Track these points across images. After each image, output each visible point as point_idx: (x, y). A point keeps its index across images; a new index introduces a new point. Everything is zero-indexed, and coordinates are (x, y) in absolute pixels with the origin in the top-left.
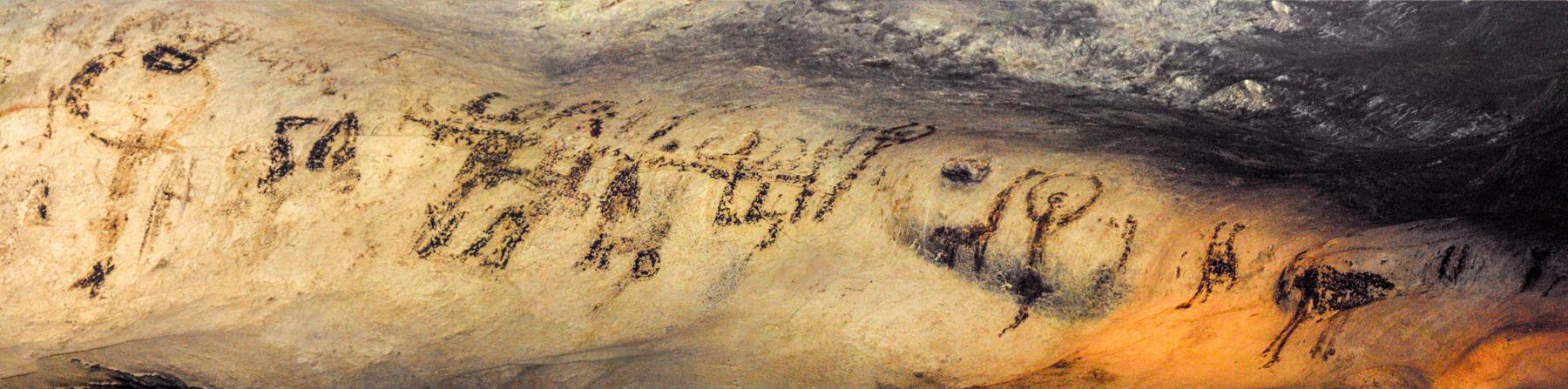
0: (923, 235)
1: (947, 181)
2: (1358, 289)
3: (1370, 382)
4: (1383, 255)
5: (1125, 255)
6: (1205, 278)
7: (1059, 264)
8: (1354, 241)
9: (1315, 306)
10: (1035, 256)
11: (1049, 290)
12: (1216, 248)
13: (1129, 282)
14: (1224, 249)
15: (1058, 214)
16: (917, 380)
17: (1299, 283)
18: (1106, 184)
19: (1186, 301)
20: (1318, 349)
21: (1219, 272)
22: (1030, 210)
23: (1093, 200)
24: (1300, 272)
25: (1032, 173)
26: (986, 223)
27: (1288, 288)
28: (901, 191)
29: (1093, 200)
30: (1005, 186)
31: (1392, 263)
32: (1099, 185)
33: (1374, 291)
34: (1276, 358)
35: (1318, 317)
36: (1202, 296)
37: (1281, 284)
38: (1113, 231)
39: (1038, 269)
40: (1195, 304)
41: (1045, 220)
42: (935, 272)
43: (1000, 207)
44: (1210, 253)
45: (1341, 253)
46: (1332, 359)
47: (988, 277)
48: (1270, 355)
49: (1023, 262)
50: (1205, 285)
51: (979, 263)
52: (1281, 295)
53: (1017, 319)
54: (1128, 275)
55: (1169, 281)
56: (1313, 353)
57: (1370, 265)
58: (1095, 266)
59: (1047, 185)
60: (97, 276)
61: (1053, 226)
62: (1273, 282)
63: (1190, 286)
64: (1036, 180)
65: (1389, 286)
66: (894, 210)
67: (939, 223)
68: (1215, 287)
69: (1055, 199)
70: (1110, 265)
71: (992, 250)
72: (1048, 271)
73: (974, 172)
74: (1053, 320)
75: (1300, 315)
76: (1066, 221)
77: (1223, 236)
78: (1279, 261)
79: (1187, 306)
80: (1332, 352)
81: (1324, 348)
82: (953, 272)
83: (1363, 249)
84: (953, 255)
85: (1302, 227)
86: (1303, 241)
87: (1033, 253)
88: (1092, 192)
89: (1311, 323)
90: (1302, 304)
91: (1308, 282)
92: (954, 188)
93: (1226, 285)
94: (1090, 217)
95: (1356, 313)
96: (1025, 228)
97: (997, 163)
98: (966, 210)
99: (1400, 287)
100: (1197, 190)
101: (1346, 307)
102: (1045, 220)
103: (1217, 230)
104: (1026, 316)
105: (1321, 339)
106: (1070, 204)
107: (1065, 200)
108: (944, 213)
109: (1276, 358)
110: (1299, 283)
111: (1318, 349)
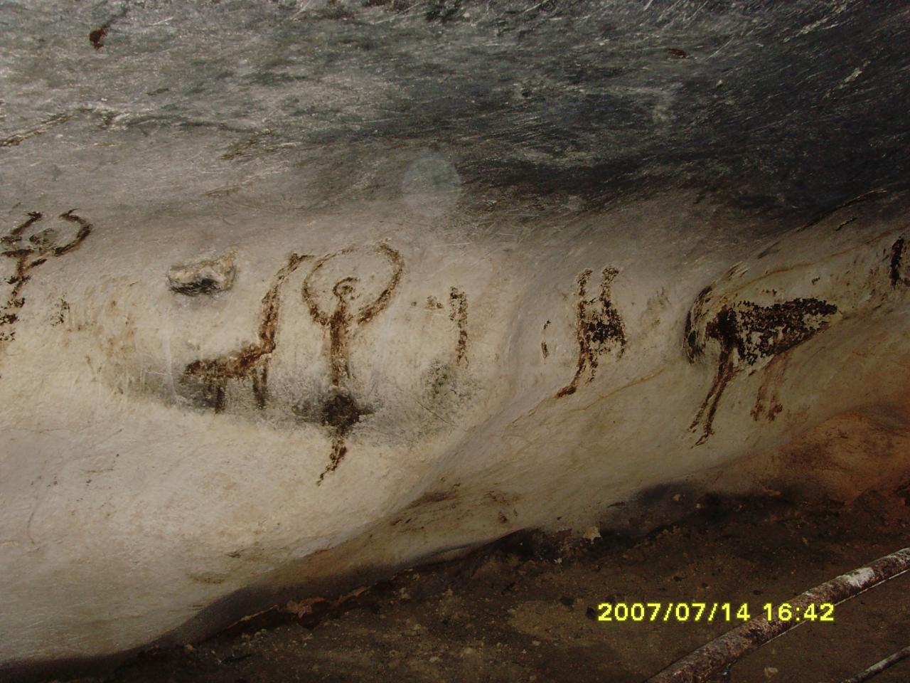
0: (169, 377)
1: (181, 298)
2: (789, 324)
3: (835, 434)
4: (812, 273)
5: (461, 342)
6: (584, 349)
7: (376, 374)
8: (771, 263)
9: (743, 356)
10: (338, 372)
11: (368, 411)
12: (588, 308)
13: (476, 376)
14: (599, 307)
15: (354, 309)
16: (235, 561)
17: (713, 331)
18: (404, 252)
19: (567, 384)
20: (760, 408)
21: (601, 338)
22: (314, 311)
23: (396, 279)
24: (711, 317)
25: (294, 261)
26: (258, 341)
27: (701, 340)
28: (112, 326)
29: (396, 279)
30: (266, 287)
31: (826, 280)
32: (395, 256)
33: (812, 321)
34: (708, 430)
35: (750, 369)
36: (587, 373)
37: (691, 338)
38: (437, 314)
39: (347, 387)
40: (581, 385)
41: (338, 319)
42: (201, 422)
43: (270, 317)
44: (582, 316)
45: (760, 285)
46: (780, 417)
47: (278, 412)
48: (700, 429)
49: (325, 382)
50: (586, 357)
51: (261, 397)
52: (693, 350)
53: (333, 458)
54: (473, 368)
55: (535, 364)
56: (755, 415)
57: (799, 290)
58: (425, 366)
59: (325, 271)
60: (40, 478)
61: (353, 327)
62: (677, 335)
63: (566, 364)
64: (304, 269)
65: (828, 310)
66: (110, 354)
67: (190, 358)
68: (601, 359)
69: (344, 288)
70: (446, 360)
71: (277, 376)
72: (362, 387)
73: (220, 278)
74: (384, 449)
75: (725, 372)
76: (368, 315)
77: (593, 291)
78: (677, 307)
79: (572, 390)
80: (778, 409)
81: (768, 405)
82: (223, 417)
83: (785, 270)
84: (220, 394)
85: (692, 254)
86: (702, 271)
87: (335, 368)
88: (390, 269)
89: (742, 377)
90: (724, 357)
91: (725, 328)
92: (195, 307)
93: (614, 352)
94: (397, 304)
95: (796, 353)
96: (317, 337)
97: (243, 262)
98: (223, 331)
99: (844, 307)
100: (527, 230)
101: (781, 349)
102: (338, 319)
103: (583, 283)
104: (343, 451)
105: (761, 396)
106: (366, 291)
107: (358, 287)
108: (194, 342)
109: (708, 430)
110: (713, 331)
111: (760, 408)
